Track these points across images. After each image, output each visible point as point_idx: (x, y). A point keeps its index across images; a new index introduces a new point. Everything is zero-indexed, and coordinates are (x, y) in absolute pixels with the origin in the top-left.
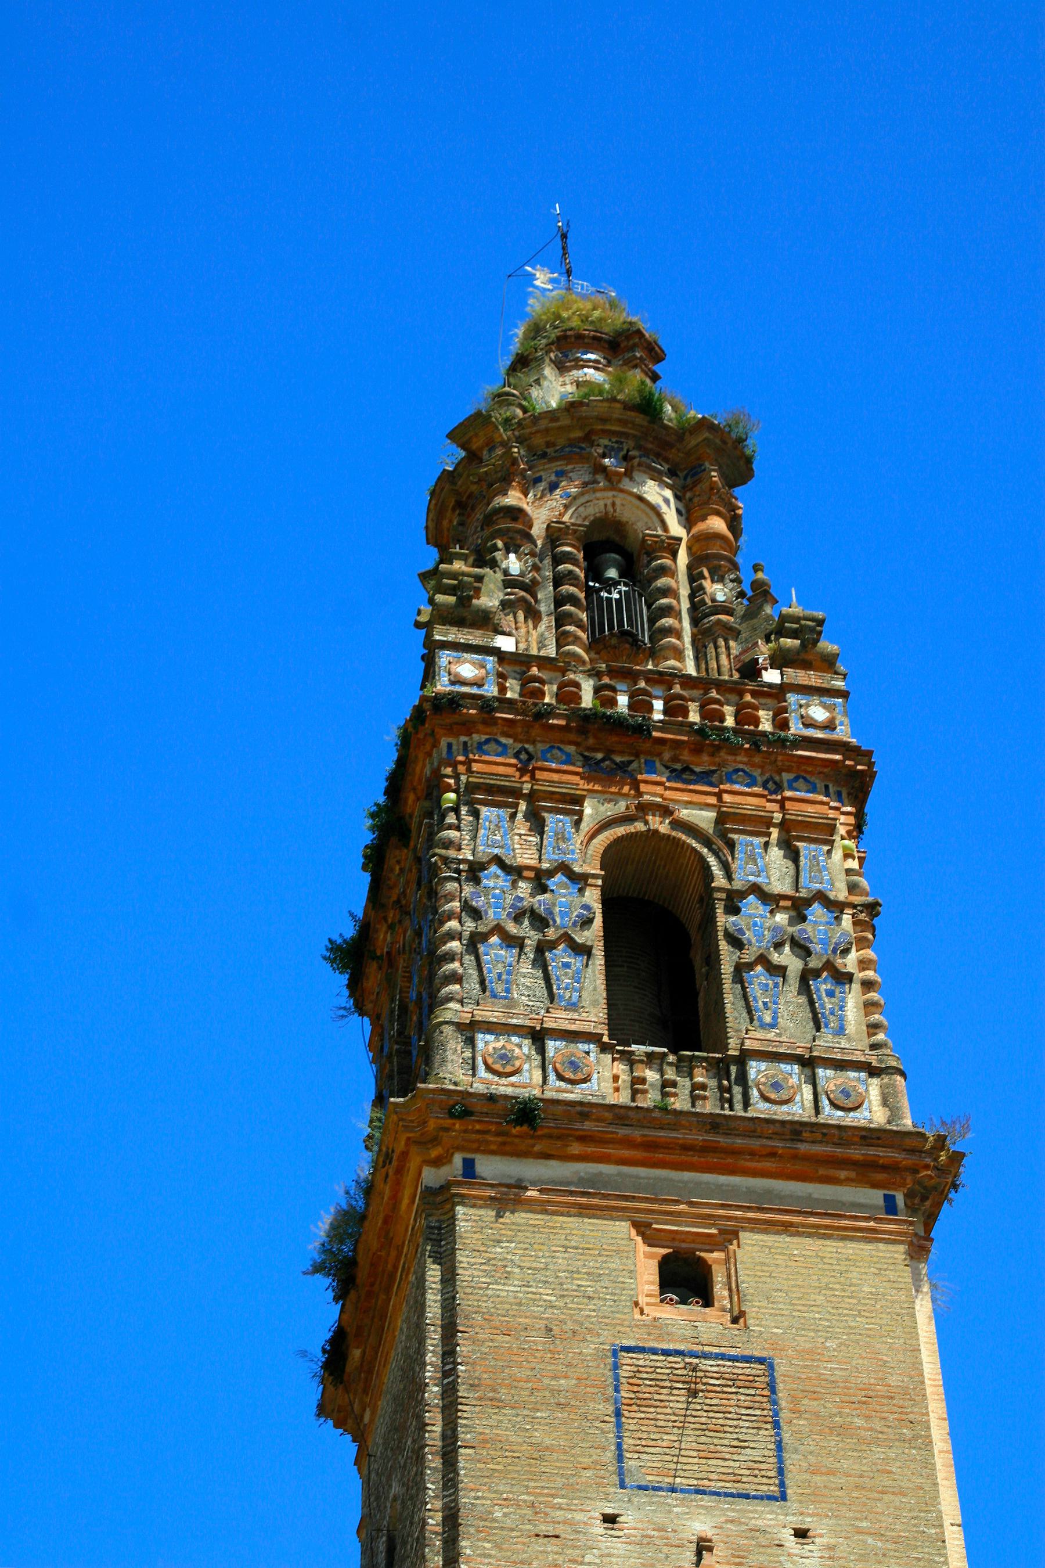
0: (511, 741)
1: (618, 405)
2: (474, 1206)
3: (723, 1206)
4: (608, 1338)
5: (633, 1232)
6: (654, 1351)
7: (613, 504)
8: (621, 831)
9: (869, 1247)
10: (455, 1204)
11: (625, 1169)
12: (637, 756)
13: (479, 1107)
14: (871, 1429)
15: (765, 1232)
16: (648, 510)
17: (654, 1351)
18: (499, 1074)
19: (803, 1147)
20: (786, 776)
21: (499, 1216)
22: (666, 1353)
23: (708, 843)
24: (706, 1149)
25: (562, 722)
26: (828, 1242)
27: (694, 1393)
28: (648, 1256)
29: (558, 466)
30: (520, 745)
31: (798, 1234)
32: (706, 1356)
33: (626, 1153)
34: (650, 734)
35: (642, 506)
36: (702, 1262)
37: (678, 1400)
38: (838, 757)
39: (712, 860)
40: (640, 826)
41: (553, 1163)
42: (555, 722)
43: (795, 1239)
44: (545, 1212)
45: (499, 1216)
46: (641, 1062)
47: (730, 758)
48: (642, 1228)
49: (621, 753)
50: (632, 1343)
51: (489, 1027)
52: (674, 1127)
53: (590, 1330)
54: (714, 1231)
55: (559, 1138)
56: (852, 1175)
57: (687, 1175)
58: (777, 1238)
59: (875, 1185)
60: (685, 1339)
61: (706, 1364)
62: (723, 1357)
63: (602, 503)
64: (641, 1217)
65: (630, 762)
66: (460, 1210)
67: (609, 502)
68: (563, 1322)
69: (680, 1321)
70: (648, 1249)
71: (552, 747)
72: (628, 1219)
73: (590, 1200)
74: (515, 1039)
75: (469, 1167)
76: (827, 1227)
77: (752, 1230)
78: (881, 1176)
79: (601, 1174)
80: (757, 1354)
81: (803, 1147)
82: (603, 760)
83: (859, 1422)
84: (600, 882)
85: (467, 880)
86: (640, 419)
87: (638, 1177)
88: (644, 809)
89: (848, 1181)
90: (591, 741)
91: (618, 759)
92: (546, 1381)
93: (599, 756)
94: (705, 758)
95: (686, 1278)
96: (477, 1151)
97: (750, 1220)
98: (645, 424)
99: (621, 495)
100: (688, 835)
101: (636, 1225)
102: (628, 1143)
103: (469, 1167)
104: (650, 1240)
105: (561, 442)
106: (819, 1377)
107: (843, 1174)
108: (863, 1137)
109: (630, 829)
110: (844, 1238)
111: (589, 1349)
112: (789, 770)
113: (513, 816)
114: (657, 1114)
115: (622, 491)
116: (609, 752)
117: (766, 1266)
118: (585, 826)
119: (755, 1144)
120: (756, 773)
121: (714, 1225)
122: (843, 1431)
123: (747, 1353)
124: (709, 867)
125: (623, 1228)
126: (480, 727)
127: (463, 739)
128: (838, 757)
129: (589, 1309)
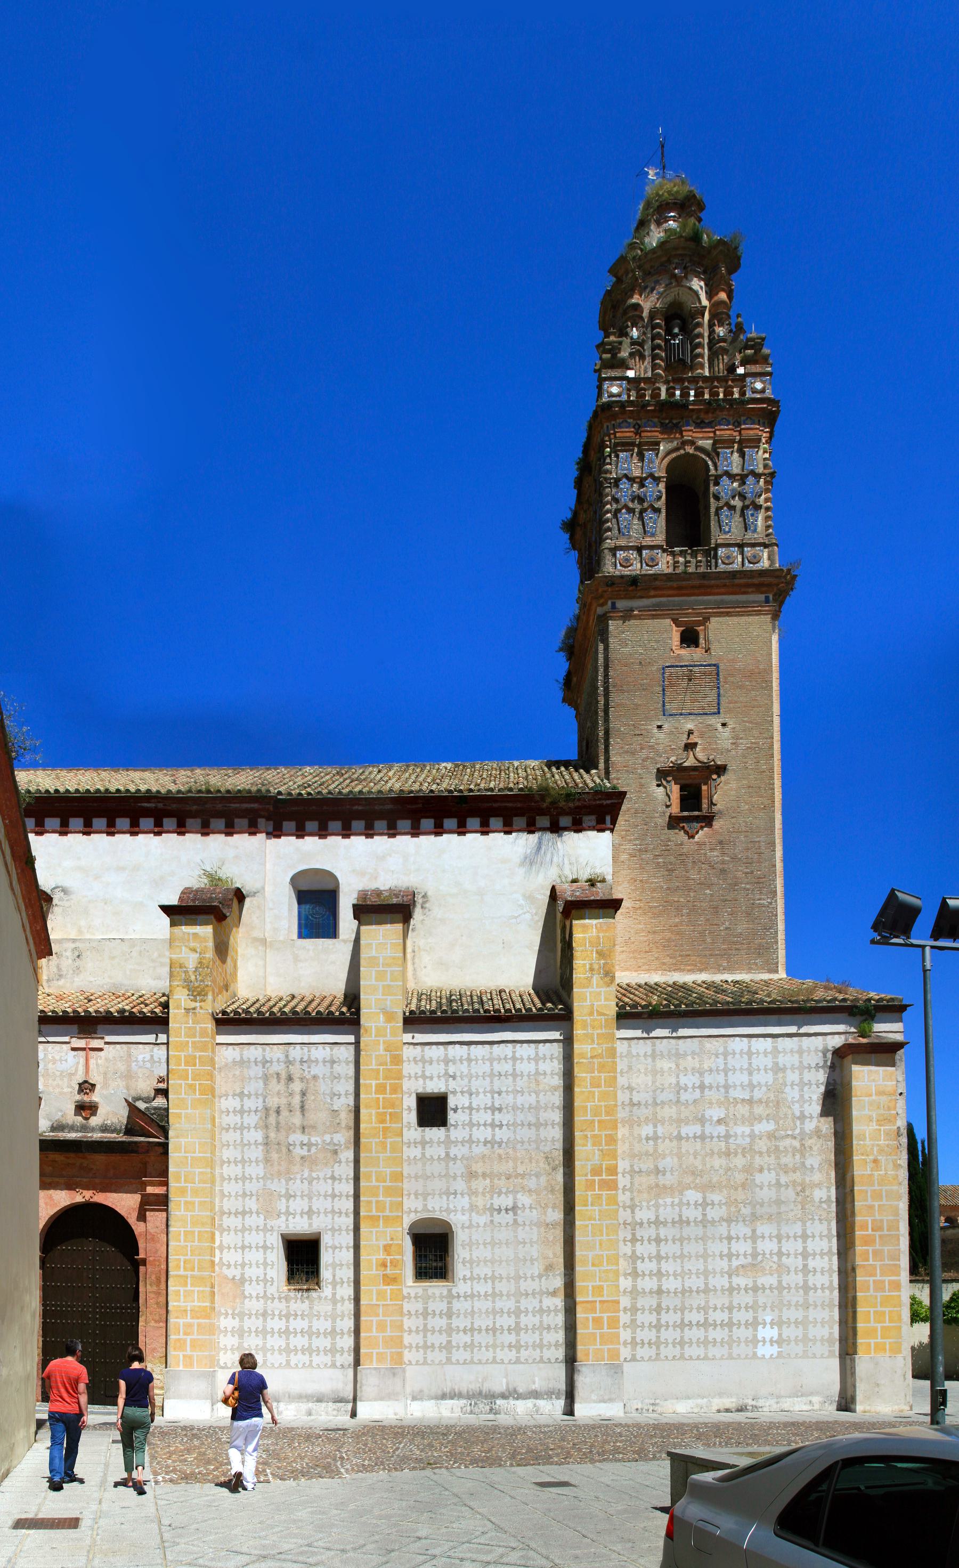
4: (661, 663)
6: (677, 666)
8: (674, 455)
12: (682, 418)
17: (677, 666)
19: (737, 581)
22: (681, 666)
23: (708, 455)
24: (700, 586)
27: (690, 680)
29: (655, 278)
32: (695, 666)
37: (684, 684)
39: (710, 463)
40: (682, 452)
61: (696, 669)
62: (701, 665)
73: (656, 613)
75: (613, 605)
81: (737, 581)
86: (692, 245)
88: (684, 443)
89: (753, 592)
91: (675, 422)
95: (690, 638)
102: (671, 588)
103: (613, 605)
107: (750, 590)
111: (654, 668)
113: (632, 455)
118: (660, 455)
119: (718, 582)
125: (668, 621)
129: (655, 654)
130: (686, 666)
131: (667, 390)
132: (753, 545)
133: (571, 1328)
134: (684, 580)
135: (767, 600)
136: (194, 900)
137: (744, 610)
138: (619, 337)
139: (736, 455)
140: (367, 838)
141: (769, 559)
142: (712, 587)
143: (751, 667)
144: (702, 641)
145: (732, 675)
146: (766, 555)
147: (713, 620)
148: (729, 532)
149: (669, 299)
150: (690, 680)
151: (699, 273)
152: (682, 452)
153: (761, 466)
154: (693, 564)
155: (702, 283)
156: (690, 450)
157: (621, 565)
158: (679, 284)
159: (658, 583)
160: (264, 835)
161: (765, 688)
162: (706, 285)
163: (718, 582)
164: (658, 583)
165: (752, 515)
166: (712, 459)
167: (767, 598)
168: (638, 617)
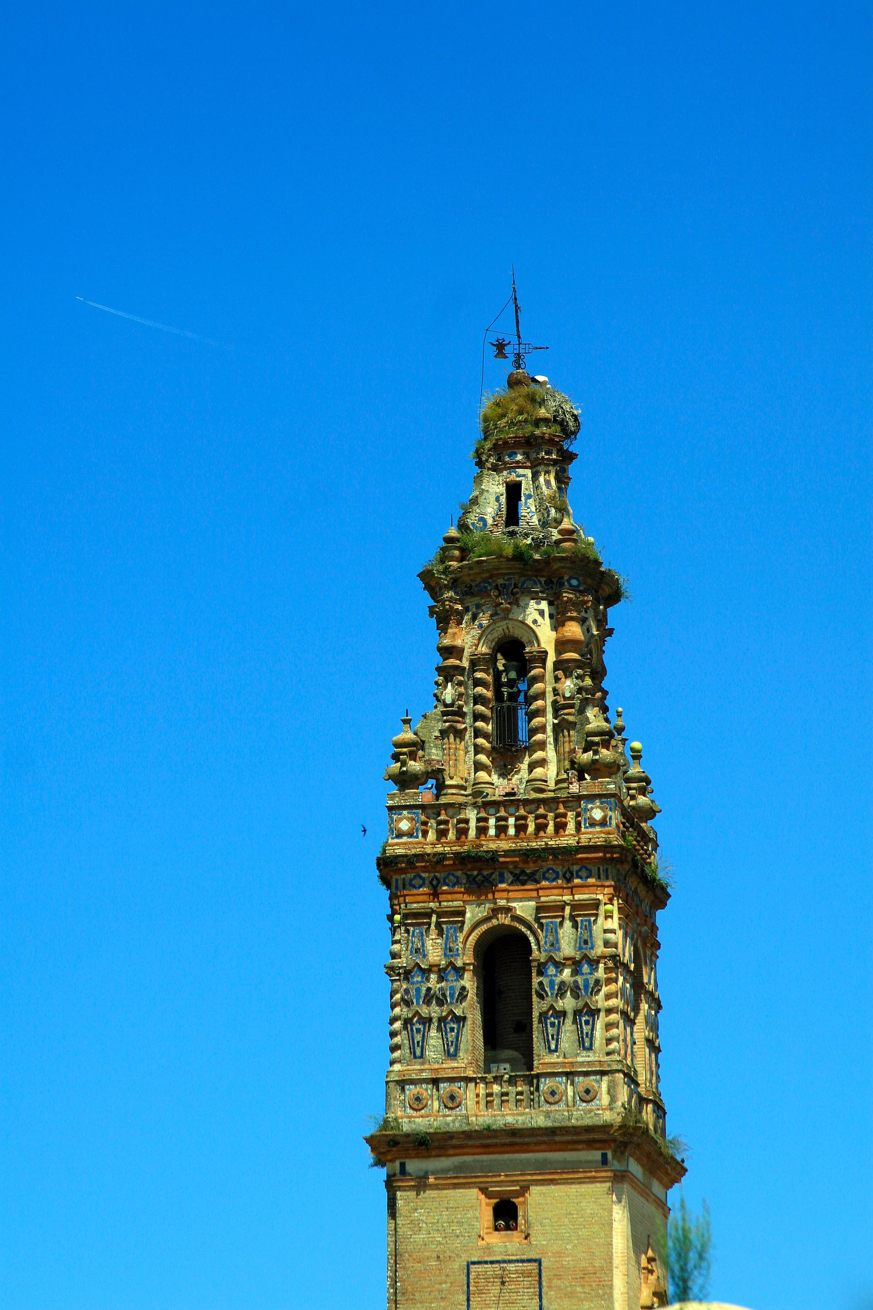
0: (427, 875)
1: (503, 559)
2: (405, 1191)
3: (521, 1175)
4: (465, 1258)
5: (480, 1193)
6: (486, 1262)
7: (508, 628)
8: (484, 927)
9: (592, 1186)
10: (396, 1191)
11: (477, 1157)
12: (495, 869)
13: (401, 1139)
14: (584, 1293)
15: (542, 1185)
16: (528, 629)
17: (486, 1262)
18: (416, 1110)
19: (557, 1138)
20: (575, 868)
21: (418, 1195)
22: (492, 1262)
23: (530, 928)
24: (512, 1144)
25: (451, 862)
26: (573, 1186)
27: (503, 1283)
28: (487, 1205)
29: (477, 600)
30: (432, 875)
31: (559, 1184)
32: (510, 1262)
33: (475, 1150)
34: (498, 861)
35: (524, 627)
36: (514, 1203)
37: (495, 1290)
38: (601, 855)
39: (532, 939)
40: (495, 922)
41: (442, 1159)
42: (447, 863)
43: (557, 1187)
44: (438, 1189)
45: (418, 1195)
46: (491, 1082)
47: (544, 864)
48: (484, 1190)
49: (487, 869)
50: (476, 1259)
51: (413, 1082)
52: (495, 1137)
53: (457, 1255)
54: (518, 1188)
55: (442, 1148)
56: (585, 1146)
57: (506, 1156)
58: (548, 1187)
59: (597, 1149)
60: (501, 1254)
61: (511, 1267)
62: (518, 1261)
63: (501, 629)
64: (482, 1186)
65: (492, 874)
66: (398, 1193)
67: (505, 627)
68: (445, 1252)
69: (504, 1244)
70: (488, 1201)
71: (449, 874)
72: (477, 1187)
73: (457, 1179)
74: (424, 1086)
75: (403, 1165)
76: (571, 1179)
77: (536, 1185)
78: (598, 1145)
79: (464, 1162)
80: (534, 1257)
81: (557, 1138)
82: (478, 875)
83: (579, 1289)
84: (471, 968)
85: (404, 979)
86: (517, 565)
87: (482, 1161)
88: (496, 911)
89: (583, 1149)
90: (469, 866)
91: (485, 873)
92: (437, 1286)
93: (475, 873)
94: (531, 865)
95: (506, 1214)
96: (406, 1157)
97: (534, 1180)
98: (521, 566)
99: (511, 622)
100: (520, 923)
101: (481, 1189)
102: (472, 1146)
103: (403, 1165)
104: (489, 1195)
105: (478, 580)
106: (562, 1266)
107: (580, 1147)
108: (586, 1130)
109: (490, 925)
110: (580, 1183)
111: (456, 1266)
112: (576, 864)
113: (428, 930)
114: (485, 1132)
115: (511, 619)
116: (480, 870)
117: (541, 1203)
118: (466, 928)
119: (534, 1140)
120: (559, 869)
121: (518, 1185)
122: (571, 1295)
123: (530, 1257)
124: (530, 944)
125: (475, 1192)
126: (410, 870)
127: (404, 876)
128: (601, 855)
129: (457, 1243)
130: (498, 1262)
131: (479, 820)
132: (586, 1074)
133: (518, 326)
134: (489, 1138)
135: (604, 1161)
136: (474, 982)
137: (569, 1174)
138: (485, 1073)
139: (568, 924)
140: (605, 675)
141: (609, 1093)
142: (527, 1144)
143: (584, 1264)
144: (521, 1220)
145: (559, 1277)
146: (604, 1086)
147: (534, 1189)
148: (556, 1051)
149: (497, 634)
150: (503, 1283)
151: (537, 592)
152: (495, 922)
153: (600, 943)
154: (502, 871)
155: (544, 605)
156: (504, 920)
157: (411, 1107)
158: (506, 618)
159: (455, 1142)
160: (659, 913)
161: (601, 1297)
162: (550, 604)
163: (534, 1140)
164: (455, 1142)
165: (587, 1023)
166: (534, 933)
167: (604, 1156)
168: (436, 1187)
